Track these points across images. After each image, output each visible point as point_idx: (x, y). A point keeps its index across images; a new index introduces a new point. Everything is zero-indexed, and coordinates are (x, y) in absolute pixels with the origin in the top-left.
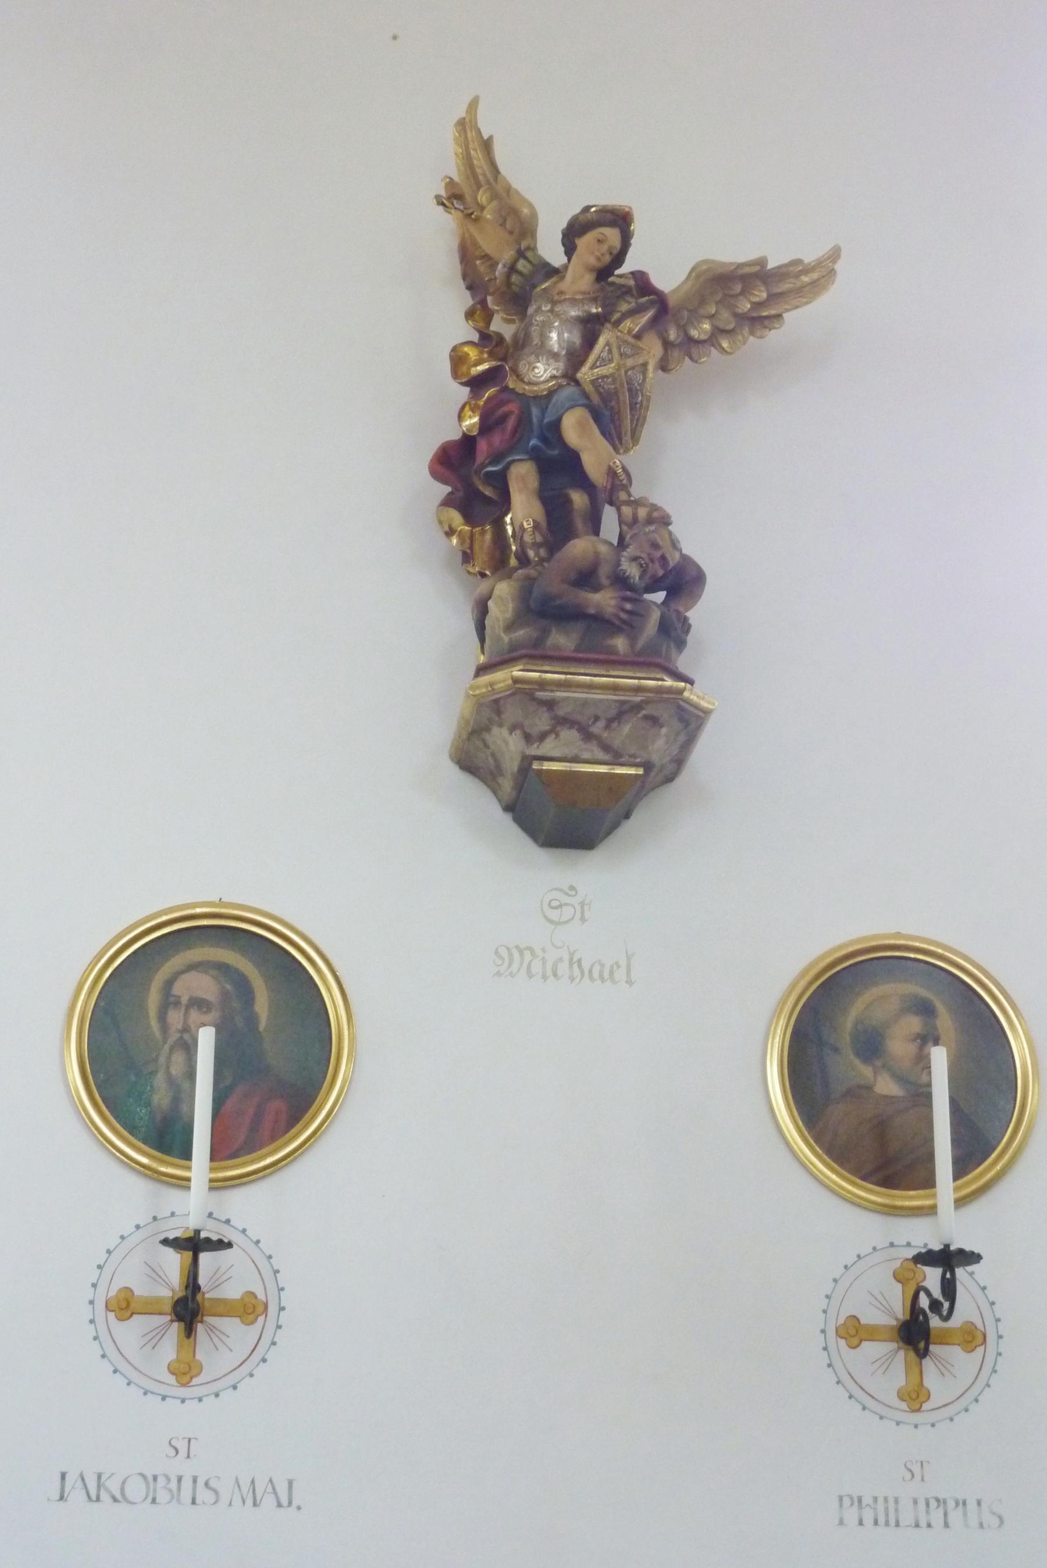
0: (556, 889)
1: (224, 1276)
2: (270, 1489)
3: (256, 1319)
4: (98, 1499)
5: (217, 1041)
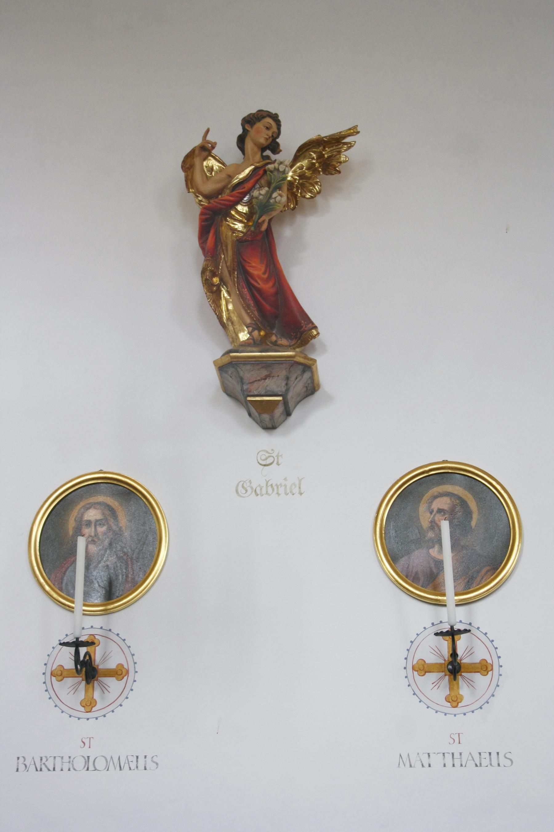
0: (262, 451)
1: (105, 657)
2: (470, 758)
3: (123, 678)
4: (41, 770)
5: (98, 539)
